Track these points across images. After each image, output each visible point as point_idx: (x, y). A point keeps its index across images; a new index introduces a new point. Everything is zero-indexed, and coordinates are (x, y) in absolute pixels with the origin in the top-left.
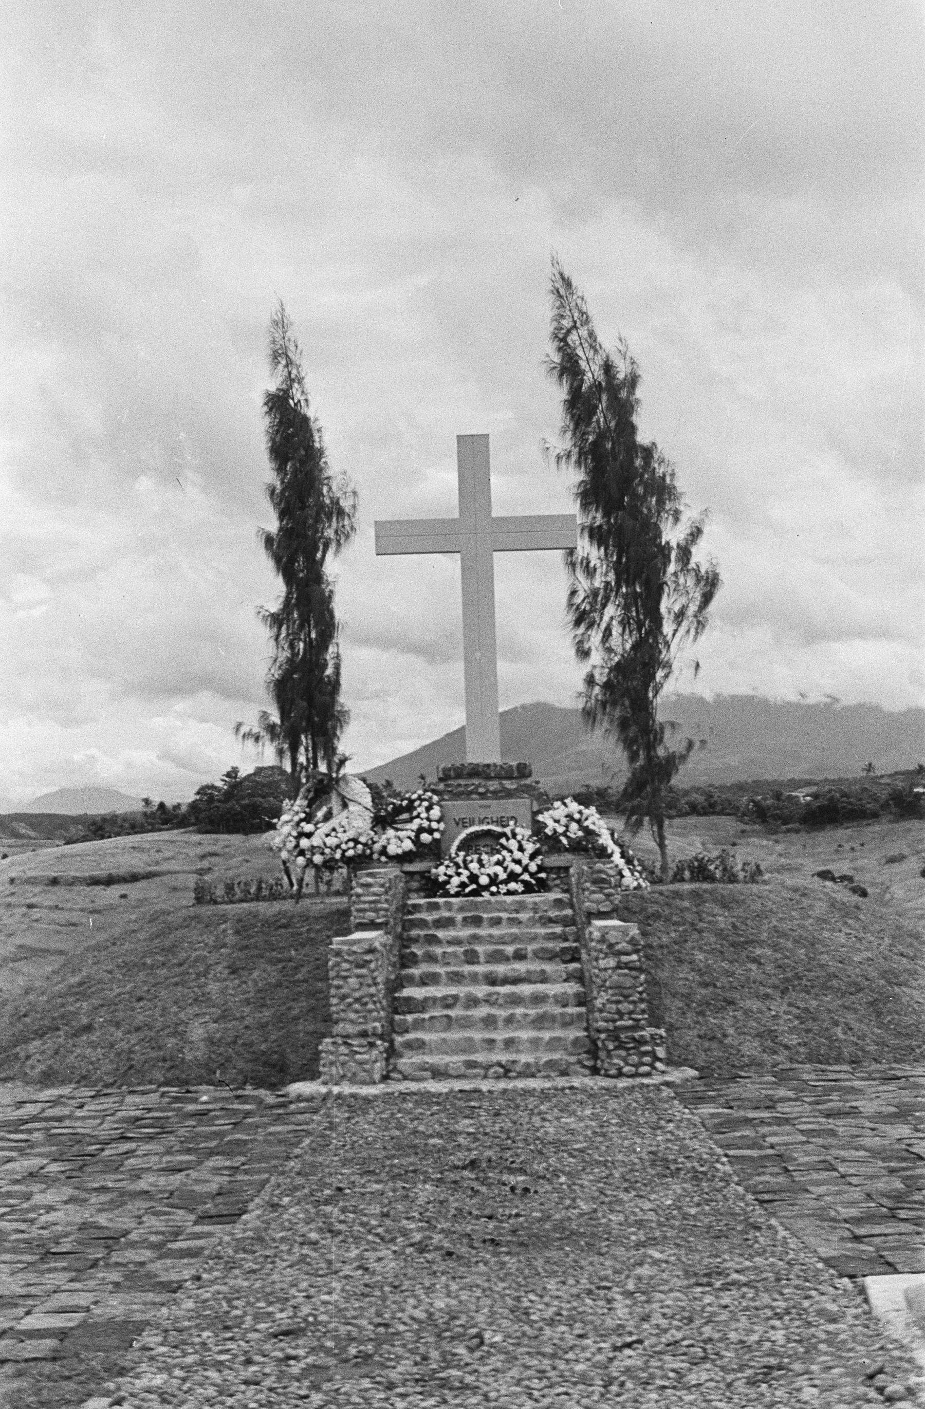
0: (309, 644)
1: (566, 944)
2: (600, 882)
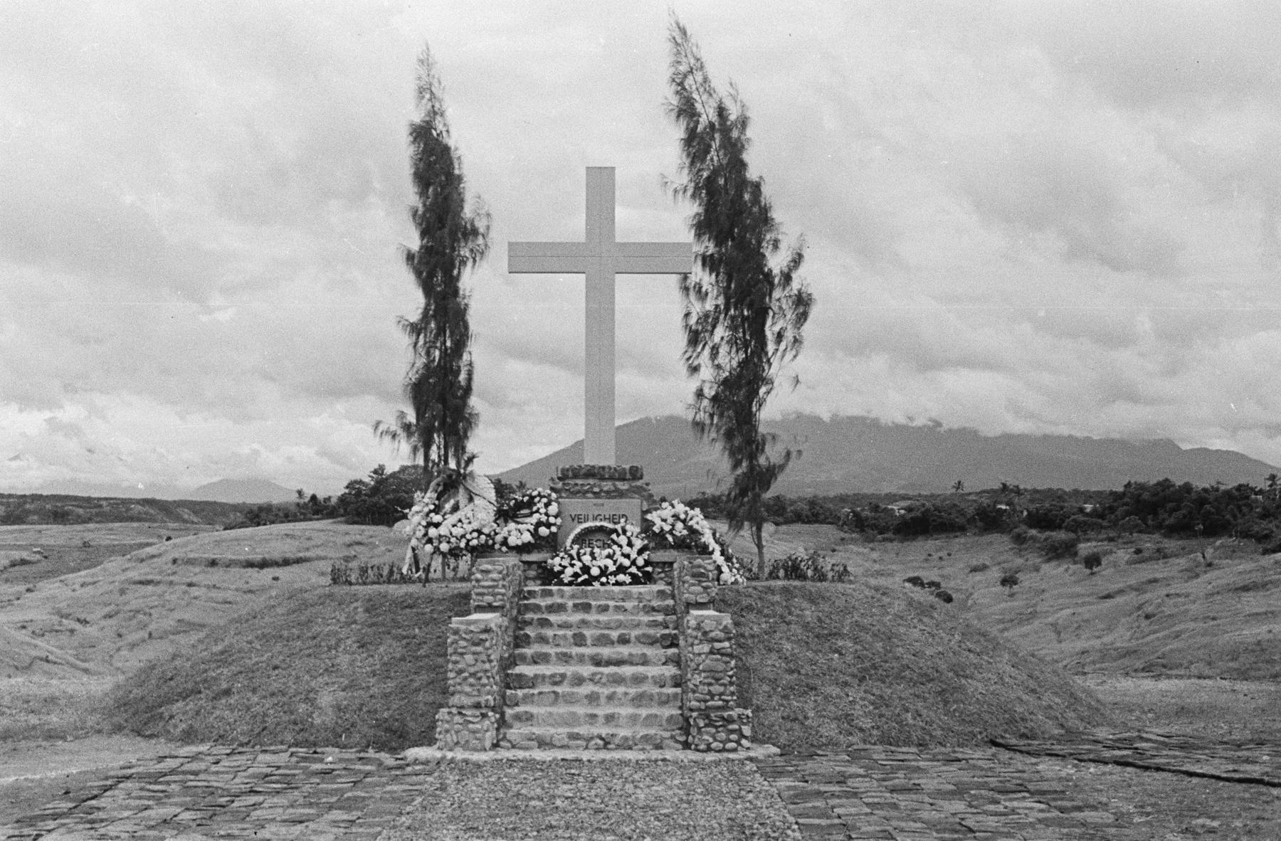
0: (444, 353)
1: (667, 631)
2: (699, 576)
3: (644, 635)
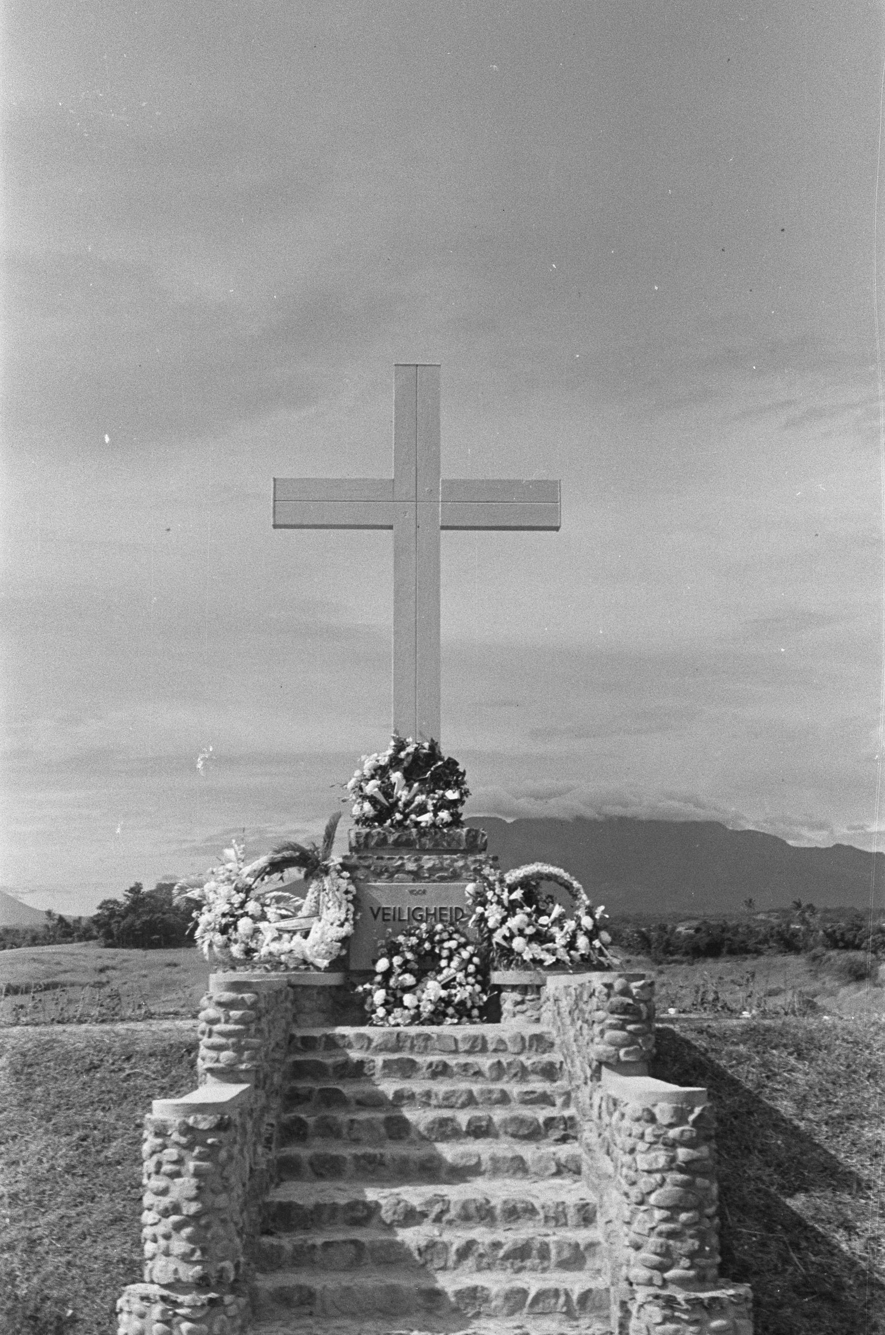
3: (514, 1119)
